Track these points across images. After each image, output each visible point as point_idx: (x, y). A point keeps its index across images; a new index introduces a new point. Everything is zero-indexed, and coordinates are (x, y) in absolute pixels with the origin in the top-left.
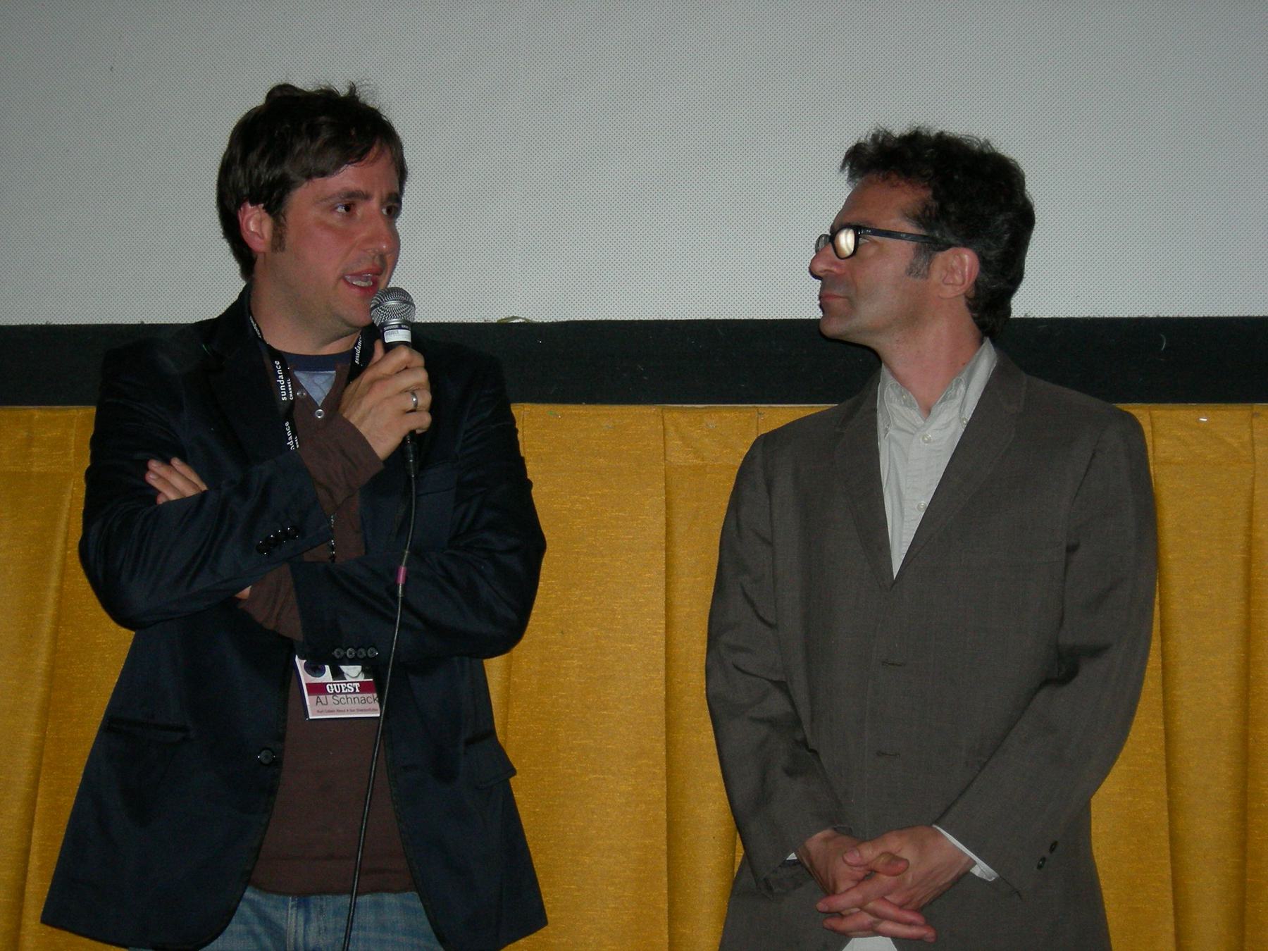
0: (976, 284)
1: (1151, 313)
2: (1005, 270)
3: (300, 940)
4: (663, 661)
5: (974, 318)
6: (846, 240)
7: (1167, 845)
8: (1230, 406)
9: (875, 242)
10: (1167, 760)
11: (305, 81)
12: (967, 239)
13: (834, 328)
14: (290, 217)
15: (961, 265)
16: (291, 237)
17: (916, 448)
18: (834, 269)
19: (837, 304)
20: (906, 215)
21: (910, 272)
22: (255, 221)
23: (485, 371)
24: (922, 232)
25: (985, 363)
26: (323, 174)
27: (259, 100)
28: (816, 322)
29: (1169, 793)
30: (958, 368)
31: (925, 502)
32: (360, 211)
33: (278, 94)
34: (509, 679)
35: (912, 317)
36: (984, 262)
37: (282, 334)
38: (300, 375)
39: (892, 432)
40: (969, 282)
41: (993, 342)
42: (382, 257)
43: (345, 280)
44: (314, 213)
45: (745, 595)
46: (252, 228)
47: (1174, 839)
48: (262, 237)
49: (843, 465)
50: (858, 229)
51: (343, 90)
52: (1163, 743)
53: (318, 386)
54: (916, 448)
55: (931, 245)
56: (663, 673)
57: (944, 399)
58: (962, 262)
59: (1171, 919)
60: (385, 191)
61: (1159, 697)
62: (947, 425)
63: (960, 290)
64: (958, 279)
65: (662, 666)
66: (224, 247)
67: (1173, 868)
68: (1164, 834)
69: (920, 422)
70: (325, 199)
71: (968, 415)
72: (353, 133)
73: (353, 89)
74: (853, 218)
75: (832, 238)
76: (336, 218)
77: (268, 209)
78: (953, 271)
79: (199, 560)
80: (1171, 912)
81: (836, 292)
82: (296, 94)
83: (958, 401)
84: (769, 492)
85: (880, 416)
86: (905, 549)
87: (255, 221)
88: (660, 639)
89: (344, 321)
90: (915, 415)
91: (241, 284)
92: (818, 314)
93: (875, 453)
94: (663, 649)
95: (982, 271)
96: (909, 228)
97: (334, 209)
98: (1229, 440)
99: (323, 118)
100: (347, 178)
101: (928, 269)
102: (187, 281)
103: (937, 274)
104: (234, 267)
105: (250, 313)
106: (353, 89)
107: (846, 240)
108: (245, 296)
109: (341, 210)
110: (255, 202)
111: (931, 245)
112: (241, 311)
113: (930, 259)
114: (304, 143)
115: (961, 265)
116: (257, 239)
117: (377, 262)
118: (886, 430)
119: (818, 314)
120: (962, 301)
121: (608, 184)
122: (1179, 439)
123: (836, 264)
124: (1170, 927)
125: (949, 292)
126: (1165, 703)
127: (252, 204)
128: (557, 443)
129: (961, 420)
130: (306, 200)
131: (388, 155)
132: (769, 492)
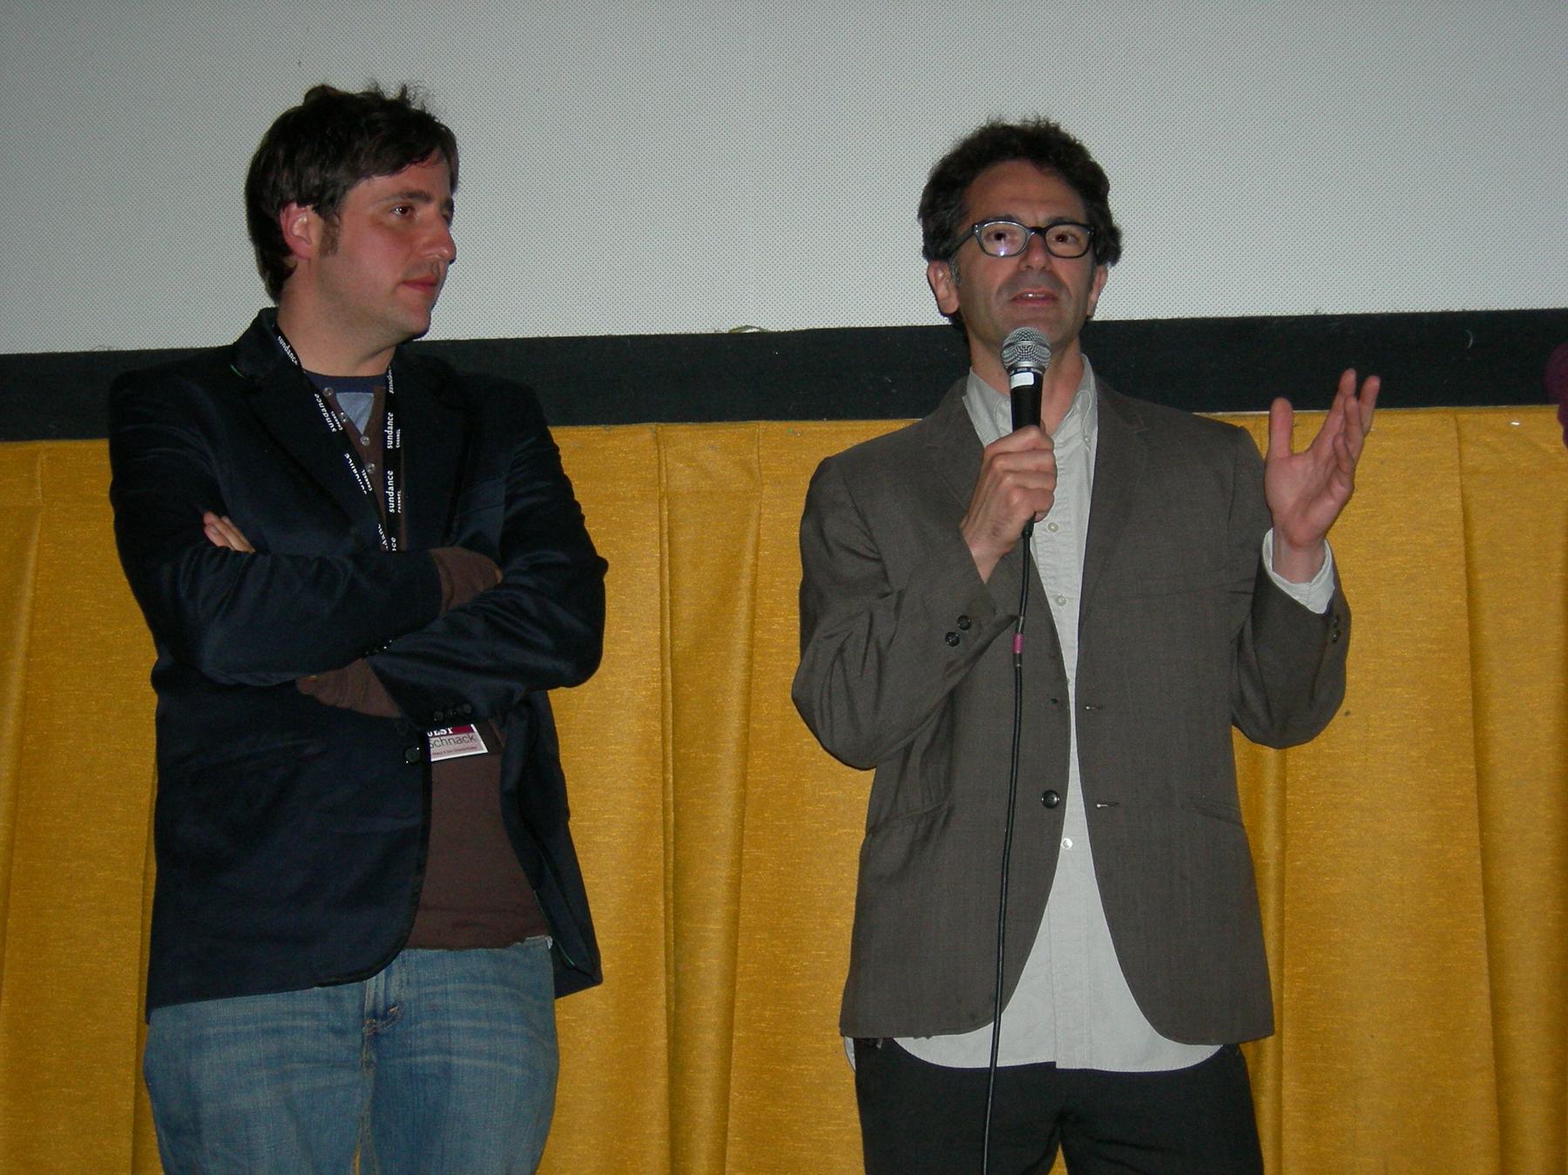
1: (1456, 307)
3: (381, 994)
7: (1480, 897)
8: (1525, 408)
10: (1480, 802)
11: (350, 83)
16: (345, 238)
22: (301, 224)
27: (298, 101)
29: (1482, 838)
30: (1075, 384)
33: (313, 98)
34: (748, 725)
37: (319, 350)
46: (297, 232)
47: (1487, 889)
51: (392, 93)
52: (1474, 785)
59: (1486, 978)
61: (1470, 734)
66: (247, 254)
67: (1487, 922)
68: (1478, 885)
73: (404, 91)
77: (317, 209)
79: (667, 571)
80: (1486, 971)
97: (392, 211)
98: (1544, 445)
100: (411, 177)
102: (201, 296)
106: (404, 91)
109: (397, 212)
110: (302, 203)
112: (265, 329)
121: (669, 196)
122: (1487, 445)
124: (1484, 988)
126: (1476, 741)
128: (605, 465)
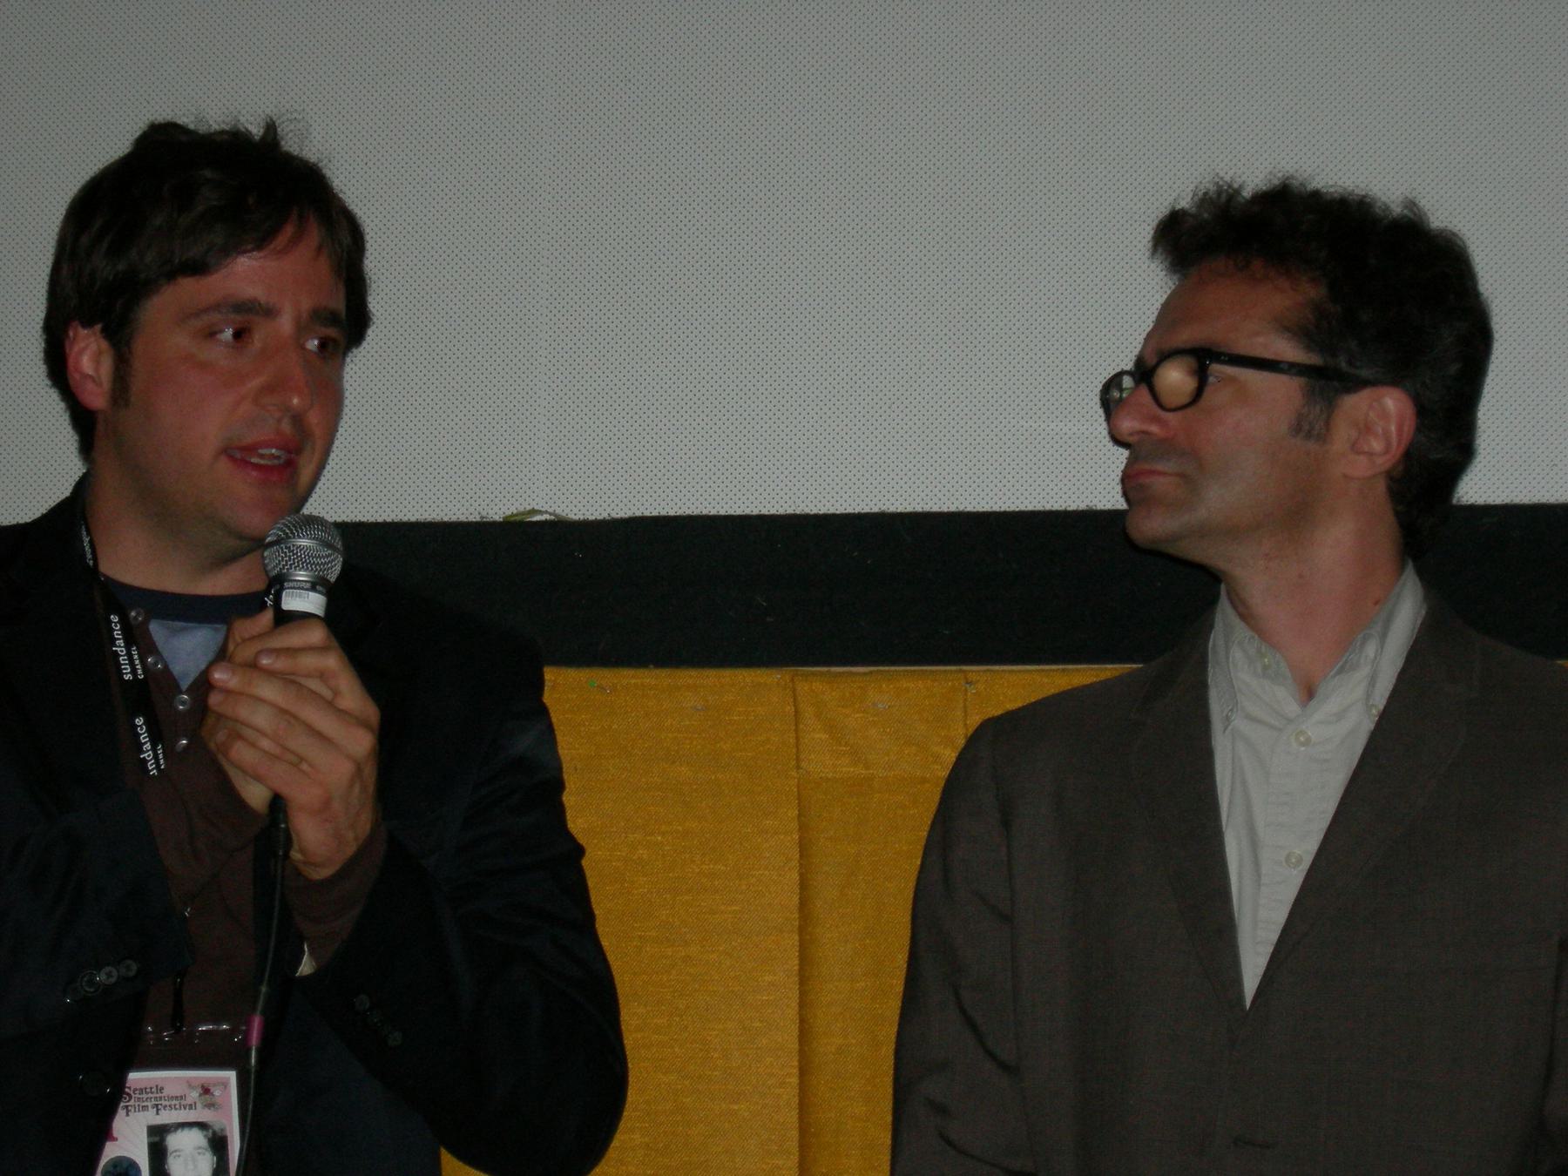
0: (1407, 455)
2: (1449, 429)
4: (795, 1134)
5: (1397, 514)
6: (1175, 377)
9: (1233, 380)
12: (1396, 375)
13: (1152, 527)
14: (139, 346)
15: (1382, 416)
17: (1286, 753)
18: (1154, 429)
19: (1160, 485)
20: (1287, 329)
21: (1297, 429)
23: (468, 625)
24: (1313, 359)
25: (1407, 610)
26: (198, 268)
28: (1113, 516)
30: (1361, 617)
31: (1307, 848)
32: (257, 340)
35: (1294, 514)
36: (1422, 411)
37: (131, 558)
38: (156, 629)
39: (1238, 723)
40: (1397, 451)
41: (1421, 573)
42: (298, 419)
43: (232, 458)
44: (180, 341)
45: (963, 1011)
48: (100, 385)
49: (1143, 782)
50: (1203, 358)
51: (256, 131)
53: (186, 650)
54: (1286, 753)
55: (1327, 381)
56: (795, 1158)
57: (1340, 672)
58: (1384, 415)
60: (306, 304)
62: (1340, 716)
63: (1384, 463)
64: (1377, 445)
65: (793, 1145)
69: (1292, 707)
70: (197, 314)
71: (1380, 699)
72: (251, 200)
73: (271, 128)
74: (1187, 336)
75: (1144, 372)
76: (219, 352)
78: (1367, 429)
81: (1159, 467)
82: (184, 138)
83: (1364, 672)
84: (1006, 824)
85: (1213, 695)
86: (1280, 916)
87: (90, 354)
88: (790, 1094)
89: (241, 537)
90: (1285, 698)
91: (74, 468)
92: (1120, 504)
93: (1207, 755)
94: (795, 1113)
95: (1418, 430)
96: (1286, 349)
97: (211, 334)
99: (208, 173)
100: (246, 274)
101: (1327, 424)
103: (1342, 433)
104: (66, 438)
105: (85, 519)
106: (271, 128)
107: (1175, 377)
108: (81, 486)
110: (87, 324)
111: (1327, 381)
112: (70, 516)
113: (1330, 406)
114: (201, 222)
115: (1382, 416)
116: (90, 386)
117: (286, 427)
118: (1227, 720)
119: (1120, 504)
120: (1381, 487)
123: (1155, 419)
125: (1360, 467)
127: (103, 330)
129: (1369, 707)
130: (165, 317)
131: (315, 234)
132: (1006, 824)
